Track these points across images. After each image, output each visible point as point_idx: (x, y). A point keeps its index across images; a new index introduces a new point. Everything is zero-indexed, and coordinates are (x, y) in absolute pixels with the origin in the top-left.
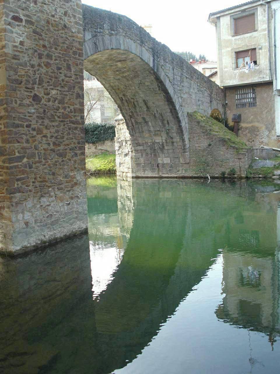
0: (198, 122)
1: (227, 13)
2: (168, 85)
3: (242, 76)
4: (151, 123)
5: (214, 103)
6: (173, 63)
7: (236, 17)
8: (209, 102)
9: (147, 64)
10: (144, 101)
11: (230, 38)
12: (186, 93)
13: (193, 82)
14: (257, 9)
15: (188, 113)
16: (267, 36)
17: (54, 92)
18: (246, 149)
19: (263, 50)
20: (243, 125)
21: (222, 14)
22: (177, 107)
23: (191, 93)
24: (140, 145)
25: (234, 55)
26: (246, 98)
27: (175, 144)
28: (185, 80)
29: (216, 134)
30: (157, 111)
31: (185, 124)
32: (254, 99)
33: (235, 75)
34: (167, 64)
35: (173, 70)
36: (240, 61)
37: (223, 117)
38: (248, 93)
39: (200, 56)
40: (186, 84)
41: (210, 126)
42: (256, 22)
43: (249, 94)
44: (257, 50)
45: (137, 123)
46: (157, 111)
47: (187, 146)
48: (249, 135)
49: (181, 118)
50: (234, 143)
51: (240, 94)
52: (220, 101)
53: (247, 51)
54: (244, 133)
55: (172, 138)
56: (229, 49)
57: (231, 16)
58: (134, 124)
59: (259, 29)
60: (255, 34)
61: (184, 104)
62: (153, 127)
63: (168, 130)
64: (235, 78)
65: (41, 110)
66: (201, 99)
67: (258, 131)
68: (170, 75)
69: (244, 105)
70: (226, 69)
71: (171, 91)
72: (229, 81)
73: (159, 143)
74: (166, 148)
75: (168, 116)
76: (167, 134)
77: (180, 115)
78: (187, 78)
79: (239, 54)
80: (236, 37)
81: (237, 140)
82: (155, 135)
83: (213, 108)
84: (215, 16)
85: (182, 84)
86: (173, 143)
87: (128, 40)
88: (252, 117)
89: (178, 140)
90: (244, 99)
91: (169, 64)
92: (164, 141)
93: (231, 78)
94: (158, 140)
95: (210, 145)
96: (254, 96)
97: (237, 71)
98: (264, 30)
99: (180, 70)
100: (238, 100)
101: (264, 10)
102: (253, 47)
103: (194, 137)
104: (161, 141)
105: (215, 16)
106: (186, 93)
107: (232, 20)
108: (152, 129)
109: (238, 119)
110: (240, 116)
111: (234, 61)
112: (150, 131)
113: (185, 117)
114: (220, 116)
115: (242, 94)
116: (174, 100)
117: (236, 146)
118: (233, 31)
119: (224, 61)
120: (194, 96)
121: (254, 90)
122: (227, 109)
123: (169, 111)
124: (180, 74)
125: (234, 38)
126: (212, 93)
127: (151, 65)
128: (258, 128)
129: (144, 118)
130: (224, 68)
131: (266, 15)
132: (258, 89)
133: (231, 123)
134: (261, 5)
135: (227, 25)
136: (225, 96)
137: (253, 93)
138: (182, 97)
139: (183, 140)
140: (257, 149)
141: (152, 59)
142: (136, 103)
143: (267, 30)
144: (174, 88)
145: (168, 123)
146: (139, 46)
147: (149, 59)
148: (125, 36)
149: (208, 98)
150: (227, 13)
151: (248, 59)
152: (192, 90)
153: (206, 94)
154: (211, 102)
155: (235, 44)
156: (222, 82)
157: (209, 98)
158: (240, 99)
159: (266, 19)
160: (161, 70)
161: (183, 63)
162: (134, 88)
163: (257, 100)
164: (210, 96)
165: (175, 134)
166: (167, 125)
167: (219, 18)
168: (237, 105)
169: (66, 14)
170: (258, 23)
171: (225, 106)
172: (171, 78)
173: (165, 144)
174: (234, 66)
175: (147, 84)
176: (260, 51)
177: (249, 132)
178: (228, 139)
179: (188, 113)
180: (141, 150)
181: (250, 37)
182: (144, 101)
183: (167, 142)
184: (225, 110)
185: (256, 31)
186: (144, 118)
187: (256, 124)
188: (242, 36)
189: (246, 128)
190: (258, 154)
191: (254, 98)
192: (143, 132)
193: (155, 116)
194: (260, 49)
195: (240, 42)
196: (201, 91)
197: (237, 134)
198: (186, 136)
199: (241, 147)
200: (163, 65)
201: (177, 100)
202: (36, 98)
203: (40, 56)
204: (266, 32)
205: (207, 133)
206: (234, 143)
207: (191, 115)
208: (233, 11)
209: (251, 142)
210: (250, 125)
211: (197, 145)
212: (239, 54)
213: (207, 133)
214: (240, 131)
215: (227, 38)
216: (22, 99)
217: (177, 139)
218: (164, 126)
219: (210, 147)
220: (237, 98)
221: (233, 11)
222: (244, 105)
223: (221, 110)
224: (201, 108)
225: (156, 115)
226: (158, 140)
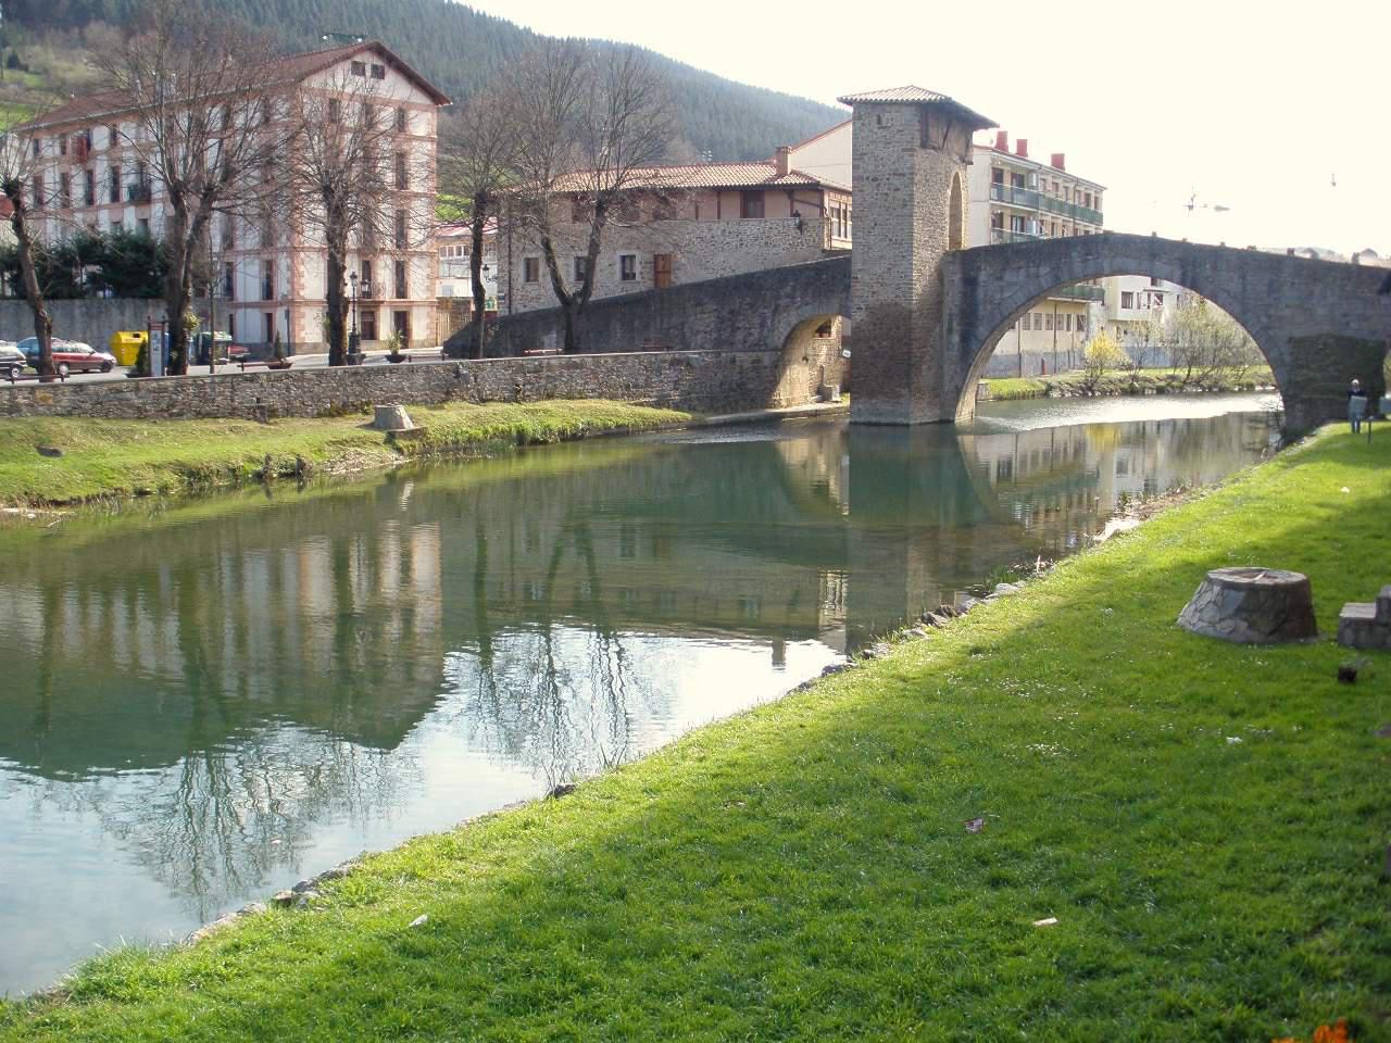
8: (902, 671)
202: (871, 347)
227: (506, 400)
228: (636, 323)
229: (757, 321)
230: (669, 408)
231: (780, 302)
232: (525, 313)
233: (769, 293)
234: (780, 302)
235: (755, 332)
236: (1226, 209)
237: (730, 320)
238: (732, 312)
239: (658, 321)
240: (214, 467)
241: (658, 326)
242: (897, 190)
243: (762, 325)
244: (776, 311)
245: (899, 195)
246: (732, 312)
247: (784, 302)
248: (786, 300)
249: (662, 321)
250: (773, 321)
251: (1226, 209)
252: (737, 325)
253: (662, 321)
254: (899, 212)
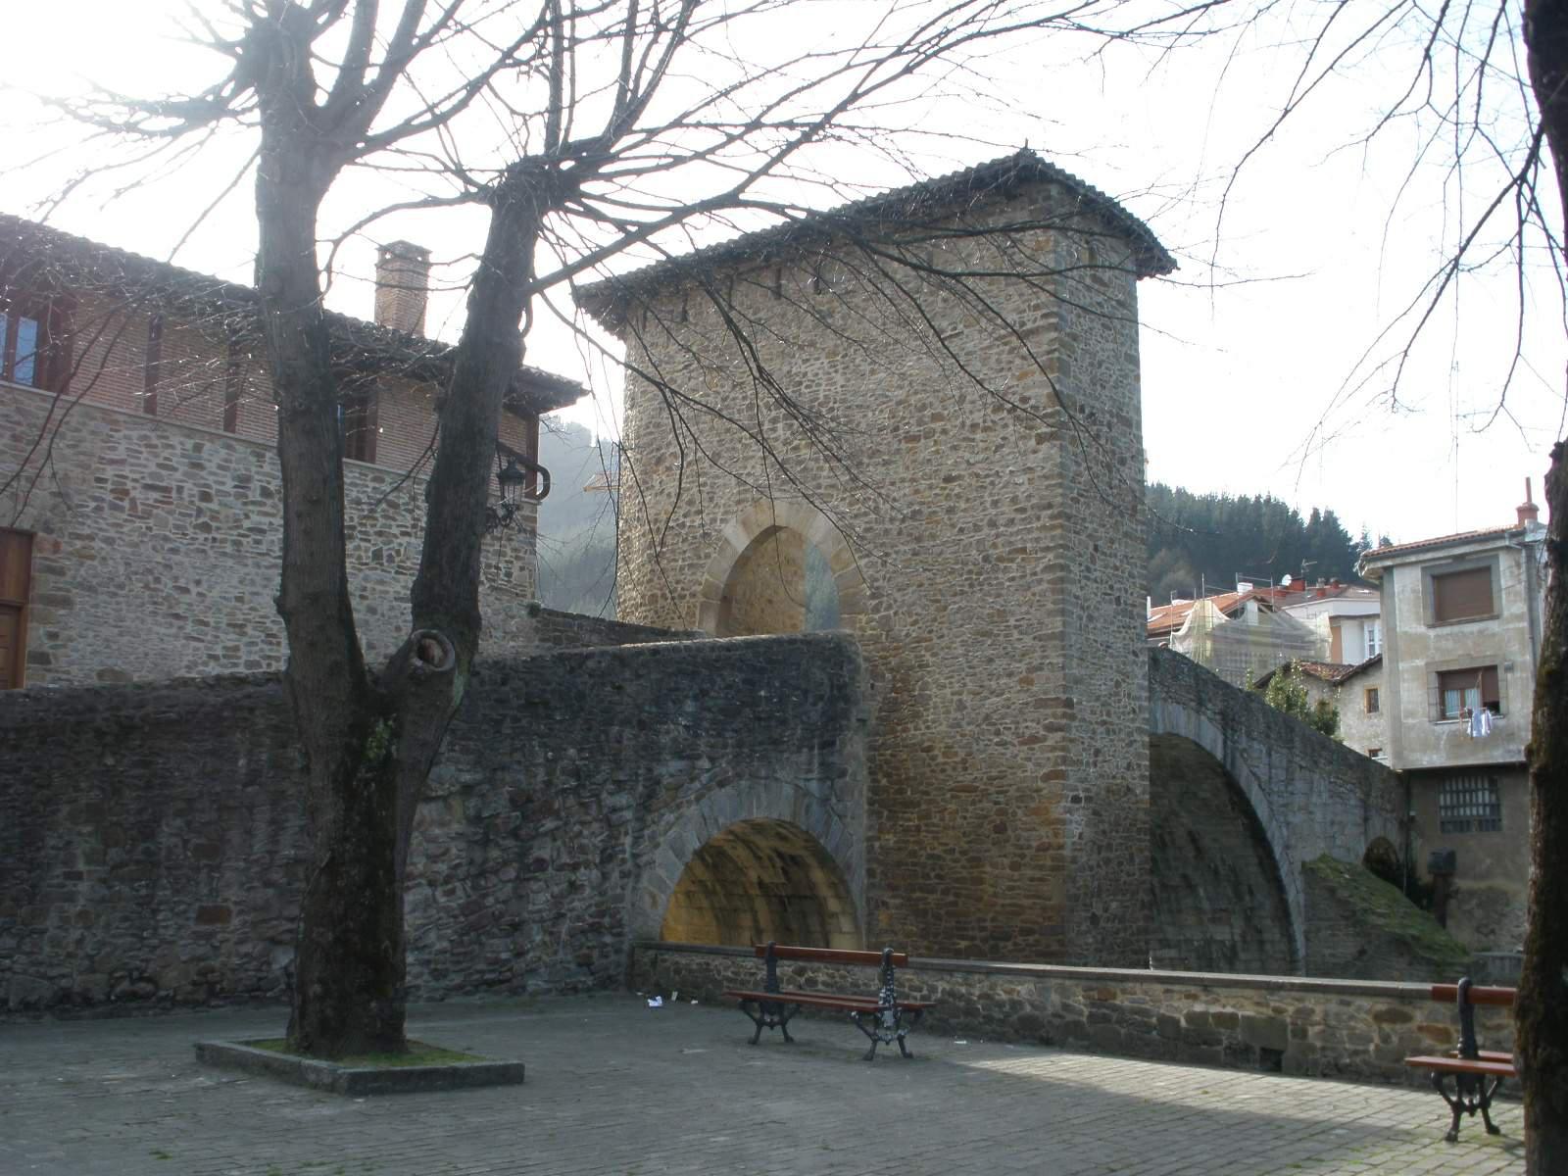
0: (1332, 891)
1: (1413, 559)
2: (1256, 797)
3: (1458, 741)
4: (1205, 890)
5: (1377, 823)
6: (1268, 736)
7: (1437, 572)
8: (1360, 821)
9: (1210, 755)
10: (1190, 833)
11: (1422, 629)
12: (1300, 809)
13: (1316, 776)
14: (1497, 557)
15: (1304, 864)
16: (1527, 636)
17: (1114, 905)
18: (1461, 965)
19: (1518, 674)
20: (1462, 883)
21: (1398, 561)
22: (1278, 851)
23: (1311, 808)
24: (1169, 946)
25: (1434, 682)
26: (1471, 805)
27: (1268, 947)
28: (1298, 774)
29: (1381, 921)
30: (1223, 861)
31: (1295, 894)
32: (1495, 807)
33: (1438, 738)
34: (1256, 745)
35: (1269, 755)
36: (1453, 697)
37: (1401, 857)
38: (1477, 790)
39: (1316, 514)
40: (1299, 785)
41: (1364, 899)
42: (1495, 595)
43: (1480, 794)
44: (1500, 672)
45: (1164, 886)
46: (1223, 861)
47: (1302, 952)
48: (1479, 913)
49: (1286, 880)
50: (1429, 948)
51: (1452, 792)
52: (1392, 811)
53: (1473, 671)
54: (1467, 907)
55: (1260, 932)
56: (1420, 662)
57: (1423, 569)
58: (1157, 891)
59: (1506, 613)
60: (1493, 626)
61: (1293, 842)
62: (1209, 899)
63: (1252, 909)
64: (1436, 748)
65: (1099, 937)
66: (1338, 818)
67: (1507, 905)
68: (1262, 771)
69: (1463, 825)
70: (1410, 721)
71: (1262, 812)
72: (1418, 755)
73: (1222, 942)
74: (1242, 956)
75: (1252, 872)
76: (1248, 919)
77: (1283, 871)
78: (1301, 767)
79: (1448, 680)
80: (1440, 631)
81: (1441, 938)
82: (1214, 920)
83: (1372, 837)
84: (1379, 565)
85: (1290, 788)
86: (1261, 943)
87: (1172, 707)
88: (1488, 861)
89: (1277, 936)
90: (1465, 805)
91: (1260, 742)
92: (1237, 938)
93: (1426, 746)
94: (1222, 933)
95: (1362, 952)
96: (1494, 798)
97: (1445, 728)
98: (1519, 618)
99: (1285, 751)
100: (1446, 807)
101: (1518, 565)
102: (1488, 663)
103: (1319, 930)
104: (1227, 937)
105: (1379, 565)
106: (1300, 809)
107: (1429, 580)
108: (1206, 905)
109: (1445, 866)
110: (1451, 858)
111: (1435, 698)
112: (1199, 911)
113: (1296, 874)
114: (1393, 857)
115: (1458, 792)
116: (1269, 835)
117: (1436, 957)
118: (1430, 612)
119: (1404, 695)
120: (1318, 816)
121: (1493, 783)
122: (1413, 834)
123: (1255, 860)
124: (1284, 764)
125: (1432, 633)
126: (1368, 795)
127: (1219, 755)
128: (1505, 893)
129: (1185, 877)
130: (1406, 717)
131: (1523, 577)
132: (1505, 782)
133: (1425, 877)
134: (1508, 548)
135: (1414, 591)
136: (1408, 794)
137: (1491, 792)
138: (1288, 824)
139: (1290, 938)
140: (1502, 958)
141: (1220, 738)
142: (1167, 838)
143: (1527, 617)
144: (1270, 803)
145: (1251, 892)
146: (1193, 715)
147: (1215, 741)
148: (1165, 700)
149: (1356, 811)
150: (1413, 559)
151: (1473, 697)
152: (1314, 799)
153: (1353, 802)
154: (1366, 820)
155: (1437, 649)
156: (1398, 755)
157: (1358, 813)
158: (1453, 807)
159: (1521, 588)
160: (1239, 761)
161: (1292, 730)
162: (1166, 802)
163: (1504, 811)
164: (1365, 805)
165: (1268, 922)
166: (1247, 898)
167: (1389, 570)
168: (1443, 823)
170: (1500, 597)
171: (1407, 825)
172: (1264, 778)
173: (1239, 945)
174: (1434, 712)
175: (1202, 795)
176: (1509, 675)
177: (1479, 905)
178: (1413, 937)
179: (1304, 864)
180: (1171, 959)
181: (1481, 632)
182: (1190, 833)
183: (1244, 941)
184: (1408, 837)
185: (1497, 617)
186: (1185, 877)
187: (1500, 883)
188: (1456, 629)
189: (1472, 893)
190: (1507, 971)
191: (1492, 806)
192: (1179, 911)
193: (1216, 872)
194: (1510, 669)
195: (1450, 645)
196: (1339, 795)
197: (1442, 921)
198: (1299, 928)
199: (1449, 960)
200: (1245, 750)
201: (1277, 834)
204: (1525, 624)
205: (1354, 919)
206: (1429, 948)
207: (1312, 869)
208: (1429, 556)
209: (1486, 935)
210: (1482, 885)
211: (1327, 952)
212: (1448, 680)
213: (1354, 919)
214: (1453, 903)
215: (1413, 631)
216: (1079, 924)
217: (1273, 934)
218: (1239, 897)
219: (1365, 958)
220: (1442, 803)
221: (1429, 556)
222: (1463, 825)
223: (1395, 837)
224: (1338, 842)
225: (1221, 868)
226: (1222, 933)
227: (875, 790)
228: (168, 833)
230: (1472, 633)
231: (660, 770)
232: (293, 638)
233: (628, 733)
234: (660, 770)
236: (1528, 480)
237: (514, 834)
238: (521, 801)
239: (262, 829)
240: (47, 1018)
241: (259, 847)
244: (646, 805)
246: (521, 801)
247: (670, 768)
248: (675, 765)
249: (277, 825)
250: (636, 841)
251: (1528, 480)
252: (537, 853)
253: (277, 825)
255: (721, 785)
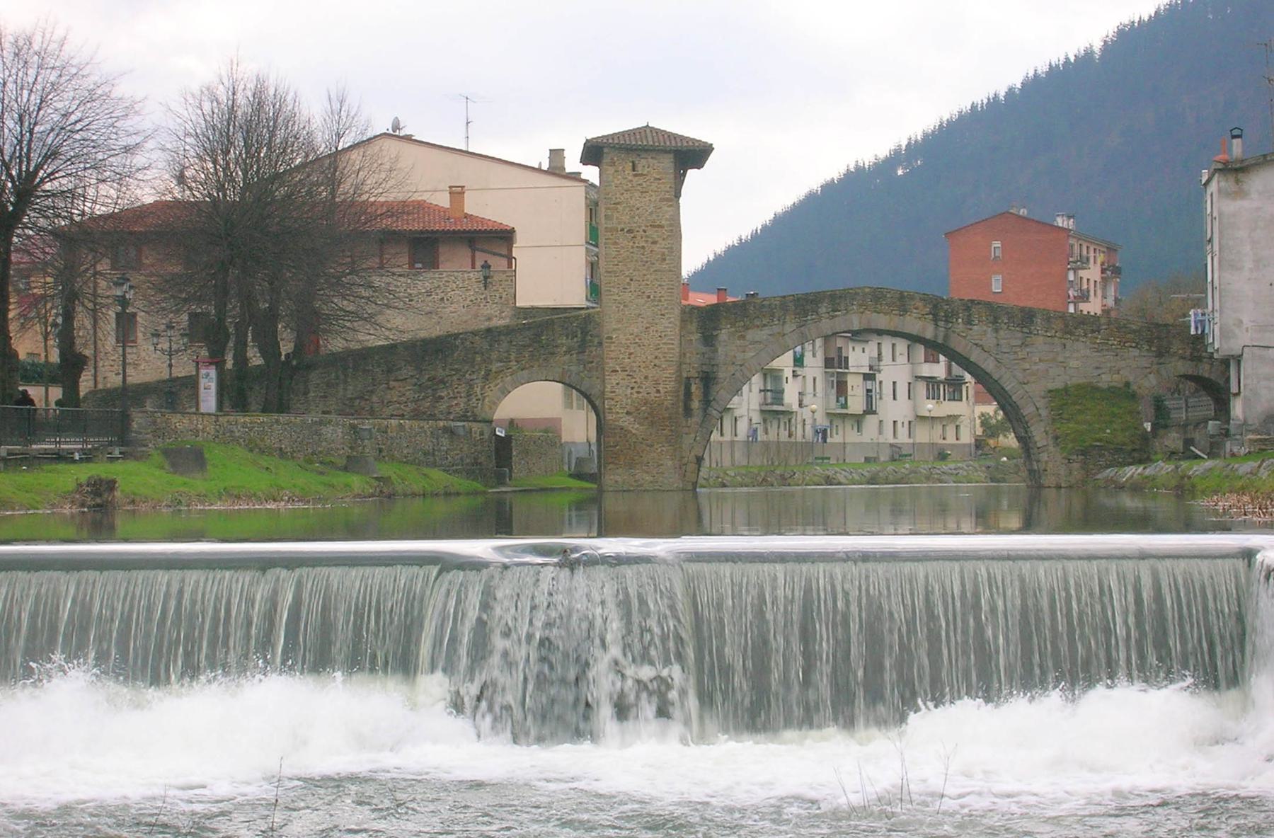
169: (656, 358)
203: (632, 388)
229: (463, 389)
235: (462, 402)
242: (655, 243)
243: (469, 395)
244: (486, 377)
245: (655, 248)
247: (495, 367)
250: (483, 388)
254: (657, 266)
255: (522, 370)
